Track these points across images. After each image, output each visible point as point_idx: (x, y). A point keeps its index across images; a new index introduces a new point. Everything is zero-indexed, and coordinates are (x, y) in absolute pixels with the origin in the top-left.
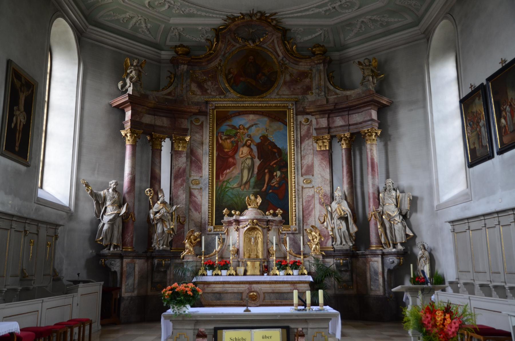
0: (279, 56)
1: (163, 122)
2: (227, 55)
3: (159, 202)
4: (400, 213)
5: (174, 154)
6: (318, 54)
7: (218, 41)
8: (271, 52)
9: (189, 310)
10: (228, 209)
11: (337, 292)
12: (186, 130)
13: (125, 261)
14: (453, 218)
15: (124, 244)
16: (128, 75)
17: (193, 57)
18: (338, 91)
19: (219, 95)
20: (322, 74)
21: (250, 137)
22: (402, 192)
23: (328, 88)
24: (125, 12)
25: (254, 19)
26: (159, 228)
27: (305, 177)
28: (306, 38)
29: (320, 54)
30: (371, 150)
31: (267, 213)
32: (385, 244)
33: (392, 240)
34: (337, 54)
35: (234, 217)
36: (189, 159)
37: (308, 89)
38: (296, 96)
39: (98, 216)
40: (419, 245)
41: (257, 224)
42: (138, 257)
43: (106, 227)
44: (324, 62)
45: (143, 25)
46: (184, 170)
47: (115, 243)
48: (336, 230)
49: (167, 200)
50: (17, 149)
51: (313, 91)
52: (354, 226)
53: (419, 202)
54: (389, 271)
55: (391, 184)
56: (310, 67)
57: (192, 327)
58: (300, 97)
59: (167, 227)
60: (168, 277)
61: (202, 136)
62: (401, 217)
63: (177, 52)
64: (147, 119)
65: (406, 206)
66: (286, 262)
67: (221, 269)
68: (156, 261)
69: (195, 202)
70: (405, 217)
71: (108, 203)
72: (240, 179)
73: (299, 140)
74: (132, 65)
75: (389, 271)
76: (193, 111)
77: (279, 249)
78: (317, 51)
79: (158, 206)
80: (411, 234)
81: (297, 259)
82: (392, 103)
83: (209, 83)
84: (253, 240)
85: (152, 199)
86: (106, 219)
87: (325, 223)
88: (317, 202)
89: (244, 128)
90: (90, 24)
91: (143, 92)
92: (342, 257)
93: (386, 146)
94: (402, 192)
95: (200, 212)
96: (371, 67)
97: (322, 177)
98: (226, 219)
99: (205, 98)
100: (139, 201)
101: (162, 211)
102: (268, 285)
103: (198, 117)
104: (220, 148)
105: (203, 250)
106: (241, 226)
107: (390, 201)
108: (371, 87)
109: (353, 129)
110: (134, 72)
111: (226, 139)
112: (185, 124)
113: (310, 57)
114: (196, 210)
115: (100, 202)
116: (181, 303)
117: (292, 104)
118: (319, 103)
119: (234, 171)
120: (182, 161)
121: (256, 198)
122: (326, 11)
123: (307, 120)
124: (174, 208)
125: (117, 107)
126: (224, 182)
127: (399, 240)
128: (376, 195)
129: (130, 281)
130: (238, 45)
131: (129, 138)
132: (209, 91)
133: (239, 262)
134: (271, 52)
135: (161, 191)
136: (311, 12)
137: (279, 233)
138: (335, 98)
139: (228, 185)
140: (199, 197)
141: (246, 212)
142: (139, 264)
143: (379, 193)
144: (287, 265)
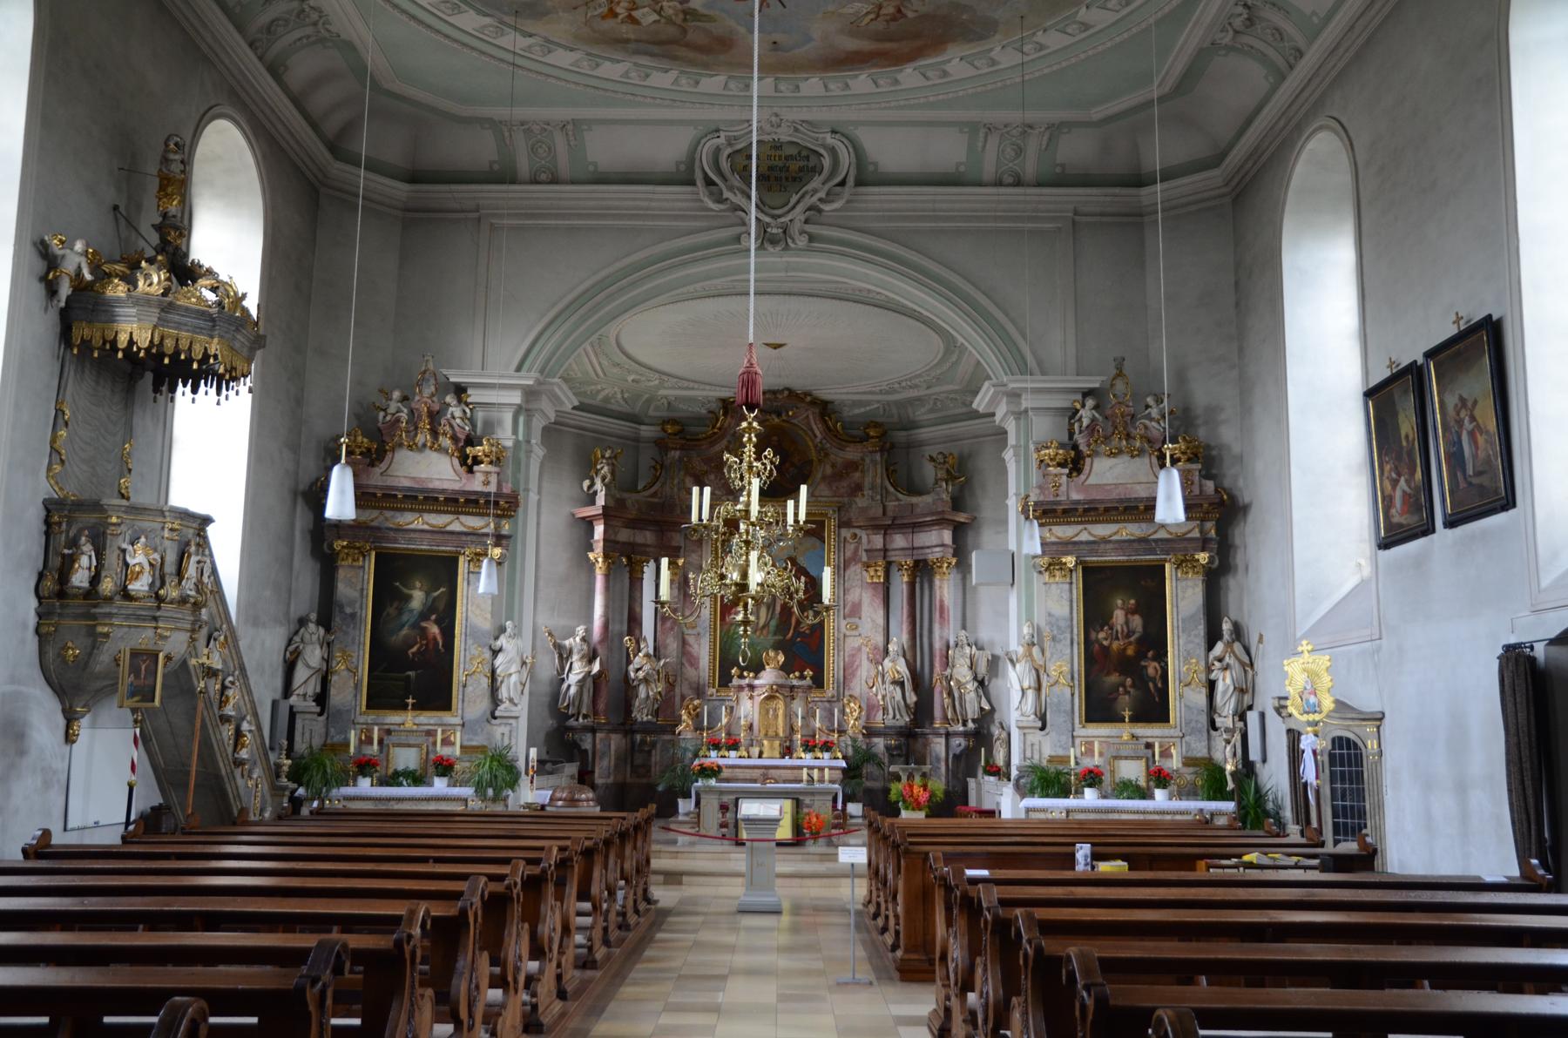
0: (816, 436)
1: (647, 537)
4: (975, 678)
6: (873, 437)
7: (725, 414)
9: (713, 782)
12: (679, 548)
13: (599, 735)
15: (596, 713)
17: (688, 437)
18: (900, 496)
19: (726, 494)
20: (879, 467)
22: (980, 648)
23: (886, 489)
27: (848, 620)
28: (857, 411)
29: (877, 437)
30: (940, 587)
31: (791, 676)
32: (953, 720)
33: (962, 715)
34: (904, 433)
35: (747, 681)
37: (857, 489)
38: (841, 499)
41: (777, 691)
42: (614, 731)
43: (573, 690)
44: (882, 450)
45: (619, 396)
47: (584, 711)
48: (888, 698)
51: (865, 493)
52: (913, 694)
54: (955, 755)
56: (861, 455)
58: (846, 500)
59: (652, 690)
60: (653, 759)
62: (976, 684)
63: (664, 430)
64: (624, 535)
65: (982, 669)
66: (815, 741)
67: (729, 749)
68: (638, 737)
70: (981, 683)
71: (575, 657)
73: (842, 566)
74: (603, 457)
77: (806, 725)
79: (638, 660)
80: (987, 707)
81: (831, 738)
82: (974, 519)
84: (771, 712)
85: (633, 650)
87: (874, 689)
88: (864, 657)
91: (618, 496)
92: (895, 737)
94: (980, 648)
95: (697, 668)
96: (947, 465)
97: (873, 621)
98: (736, 681)
101: (646, 668)
105: (705, 723)
109: (919, 555)
110: (606, 469)
114: (692, 665)
115: (564, 655)
116: (709, 777)
117: (834, 511)
118: (872, 513)
123: (855, 536)
124: (662, 662)
127: (970, 716)
128: (944, 652)
129: (605, 763)
131: (600, 565)
133: (752, 740)
135: (645, 639)
137: (807, 702)
138: (895, 506)
140: (696, 646)
141: (763, 674)
143: (948, 647)
144: (815, 746)
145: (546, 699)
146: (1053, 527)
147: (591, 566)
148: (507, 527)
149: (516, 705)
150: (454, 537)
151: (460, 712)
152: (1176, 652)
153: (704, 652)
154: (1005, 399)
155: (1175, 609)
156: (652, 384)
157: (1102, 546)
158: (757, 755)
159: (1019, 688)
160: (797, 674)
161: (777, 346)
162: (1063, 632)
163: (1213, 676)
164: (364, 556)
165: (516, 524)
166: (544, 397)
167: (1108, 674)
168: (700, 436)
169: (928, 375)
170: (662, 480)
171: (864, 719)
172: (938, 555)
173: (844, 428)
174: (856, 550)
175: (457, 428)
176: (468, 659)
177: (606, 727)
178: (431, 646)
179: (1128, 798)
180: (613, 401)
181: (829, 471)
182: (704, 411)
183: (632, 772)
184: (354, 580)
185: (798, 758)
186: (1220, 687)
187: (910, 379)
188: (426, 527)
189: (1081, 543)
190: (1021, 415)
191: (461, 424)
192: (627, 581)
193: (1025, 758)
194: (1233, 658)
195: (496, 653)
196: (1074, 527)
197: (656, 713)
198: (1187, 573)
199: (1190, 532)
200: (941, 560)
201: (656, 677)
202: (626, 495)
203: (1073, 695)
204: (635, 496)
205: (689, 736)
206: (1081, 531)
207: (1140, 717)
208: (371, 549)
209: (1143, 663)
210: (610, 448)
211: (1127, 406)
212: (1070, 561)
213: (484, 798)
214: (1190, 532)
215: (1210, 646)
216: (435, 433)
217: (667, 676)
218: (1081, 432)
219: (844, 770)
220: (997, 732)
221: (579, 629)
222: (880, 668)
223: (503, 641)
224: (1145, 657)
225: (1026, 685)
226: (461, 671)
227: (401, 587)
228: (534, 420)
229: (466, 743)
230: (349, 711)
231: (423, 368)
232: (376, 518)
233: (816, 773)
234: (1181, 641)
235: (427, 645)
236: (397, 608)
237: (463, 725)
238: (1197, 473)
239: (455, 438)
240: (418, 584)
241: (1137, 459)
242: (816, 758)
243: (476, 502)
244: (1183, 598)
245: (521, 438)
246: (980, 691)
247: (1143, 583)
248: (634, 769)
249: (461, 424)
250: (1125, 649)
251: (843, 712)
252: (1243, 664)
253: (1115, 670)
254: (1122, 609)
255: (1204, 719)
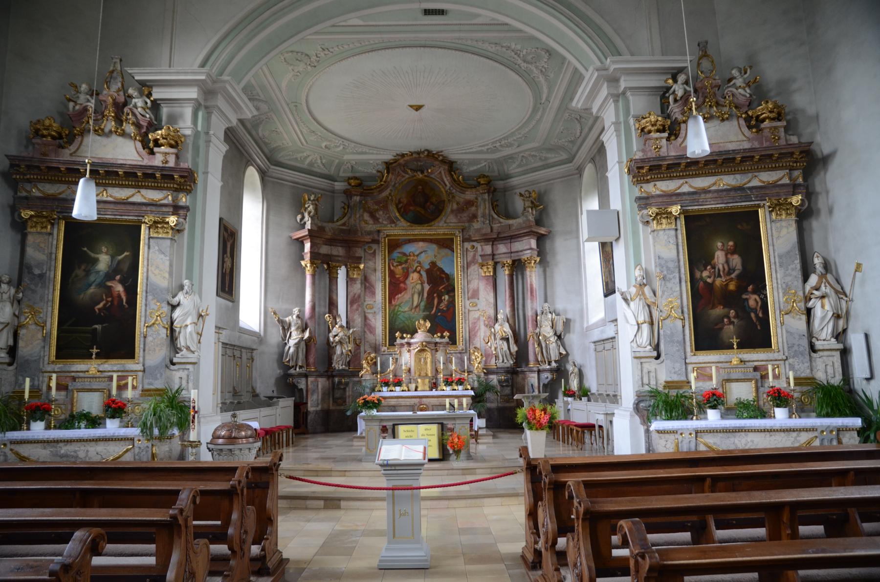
0: (446, 185)
1: (339, 251)
2: (397, 185)
3: (337, 326)
4: (555, 334)
5: (350, 280)
6: (482, 184)
7: (388, 173)
8: (439, 182)
9: (374, 412)
10: (400, 332)
11: (500, 405)
12: (360, 258)
13: (310, 379)
14: (596, 339)
15: (308, 365)
16: (306, 209)
18: (501, 220)
20: (487, 203)
21: (420, 263)
22: (558, 315)
24: (303, 152)
25: (422, 156)
26: (338, 350)
27: (471, 300)
28: (472, 169)
32: (542, 362)
33: (548, 358)
34: (502, 182)
35: (406, 340)
36: (363, 286)
37: (474, 217)
38: (463, 224)
39: (284, 339)
40: (571, 362)
41: (426, 346)
42: (321, 376)
43: (292, 350)
44: (488, 192)
45: (319, 161)
46: (359, 296)
47: (300, 364)
49: (344, 324)
50: (227, 289)
52: (515, 346)
53: (572, 324)
54: (544, 385)
55: (547, 308)
57: (378, 423)
58: (467, 225)
60: (347, 394)
61: (375, 263)
62: (556, 338)
63: (350, 184)
64: (324, 250)
65: (560, 328)
68: (336, 380)
69: (370, 326)
70: (559, 337)
71: (293, 329)
72: (411, 303)
74: (309, 199)
75: (544, 385)
76: (366, 240)
78: (482, 181)
79: (336, 330)
80: (564, 353)
81: (462, 376)
82: (550, 232)
83: (381, 213)
84: (422, 360)
86: (292, 342)
87: (489, 344)
88: (482, 323)
89: (414, 255)
90: (272, 164)
91: (320, 225)
93: (545, 271)
94: (558, 315)
95: (374, 335)
97: (487, 300)
98: (399, 341)
99: (376, 227)
100: (319, 325)
101: (341, 334)
102: (436, 399)
103: (371, 245)
104: (392, 274)
105: (379, 369)
106: (411, 348)
107: (546, 323)
108: (531, 218)
110: (311, 207)
111: (397, 265)
112: (359, 252)
113: (475, 187)
114: (371, 332)
115: (286, 328)
116: (371, 408)
118: (484, 231)
119: (405, 296)
120: (357, 287)
121: (425, 321)
122: (487, 149)
123: (473, 247)
124: (351, 331)
125: (297, 239)
126: (396, 306)
127: (553, 358)
128: (535, 318)
129: (315, 397)
130: (407, 176)
131: (309, 268)
132: (380, 220)
134: (439, 182)
135: (339, 316)
136: (475, 150)
137: (446, 353)
139: (400, 309)
140: (373, 320)
141: (416, 335)
142: (322, 383)
143: (537, 315)
144: (452, 382)
145: (276, 357)
146: (657, 183)
147: (303, 269)
148: (184, 199)
149: (193, 352)
150: (135, 208)
151: (141, 359)
152: (775, 285)
153: (379, 324)
154: (605, 85)
155: (771, 248)
156: (339, 149)
157: (703, 196)
158: (414, 389)
159: (635, 323)
160: (439, 334)
161: (418, 108)
162: (673, 272)
163: (810, 304)
164: (52, 225)
165: (195, 199)
166: (219, 96)
167: (713, 307)
168: (372, 187)
169: (520, 134)
170: (348, 215)
171: (483, 363)
172: (529, 256)
173: (463, 177)
174: (474, 256)
175: (139, 117)
176: (148, 313)
177: (315, 374)
178: (116, 303)
179: (751, 418)
180: (316, 165)
181: (455, 206)
182: (374, 172)
183: (333, 402)
184: (42, 245)
185: (441, 390)
186: (818, 313)
187: (504, 138)
188: (110, 199)
189: (684, 194)
190: (618, 97)
191: (143, 112)
192: (328, 280)
193: (643, 384)
194: (828, 287)
195: (174, 307)
196: (677, 181)
197: (349, 364)
198: (781, 215)
199: (780, 179)
200: (530, 259)
201: (347, 340)
202: (325, 224)
203: (684, 327)
204: (330, 225)
205: (368, 378)
206: (683, 184)
207: (747, 343)
208: (59, 219)
209: (744, 296)
210: (313, 193)
211: (715, 79)
212: (675, 209)
213: (150, 438)
214: (780, 179)
215: (806, 278)
216: (119, 120)
217: (355, 340)
218: (676, 101)
219: (473, 397)
220: (571, 369)
221: (294, 310)
222: (493, 330)
223: (181, 297)
224: (745, 291)
225: (641, 320)
226: (143, 323)
227: (88, 252)
228: (213, 116)
229: (147, 387)
230: (37, 361)
231: (111, 68)
232: (63, 192)
233: (456, 402)
234: (778, 275)
235: (112, 301)
236: (84, 270)
237: (144, 371)
238: (783, 129)
239: (138, 125)
240: (104, 249)
241: (726, 122)
242: (466, 389)
243: (153, 176)
244: (778, 238)
245: (199, 129)
246: (559, 342)
247: (739, 226)
248: (335, 401)
249: (143, 112)
250: (727, 285)
251: (469, 359)
252: (837, 292)
253: (720, 304)
254: (722, 250)
255: (805, 343)
